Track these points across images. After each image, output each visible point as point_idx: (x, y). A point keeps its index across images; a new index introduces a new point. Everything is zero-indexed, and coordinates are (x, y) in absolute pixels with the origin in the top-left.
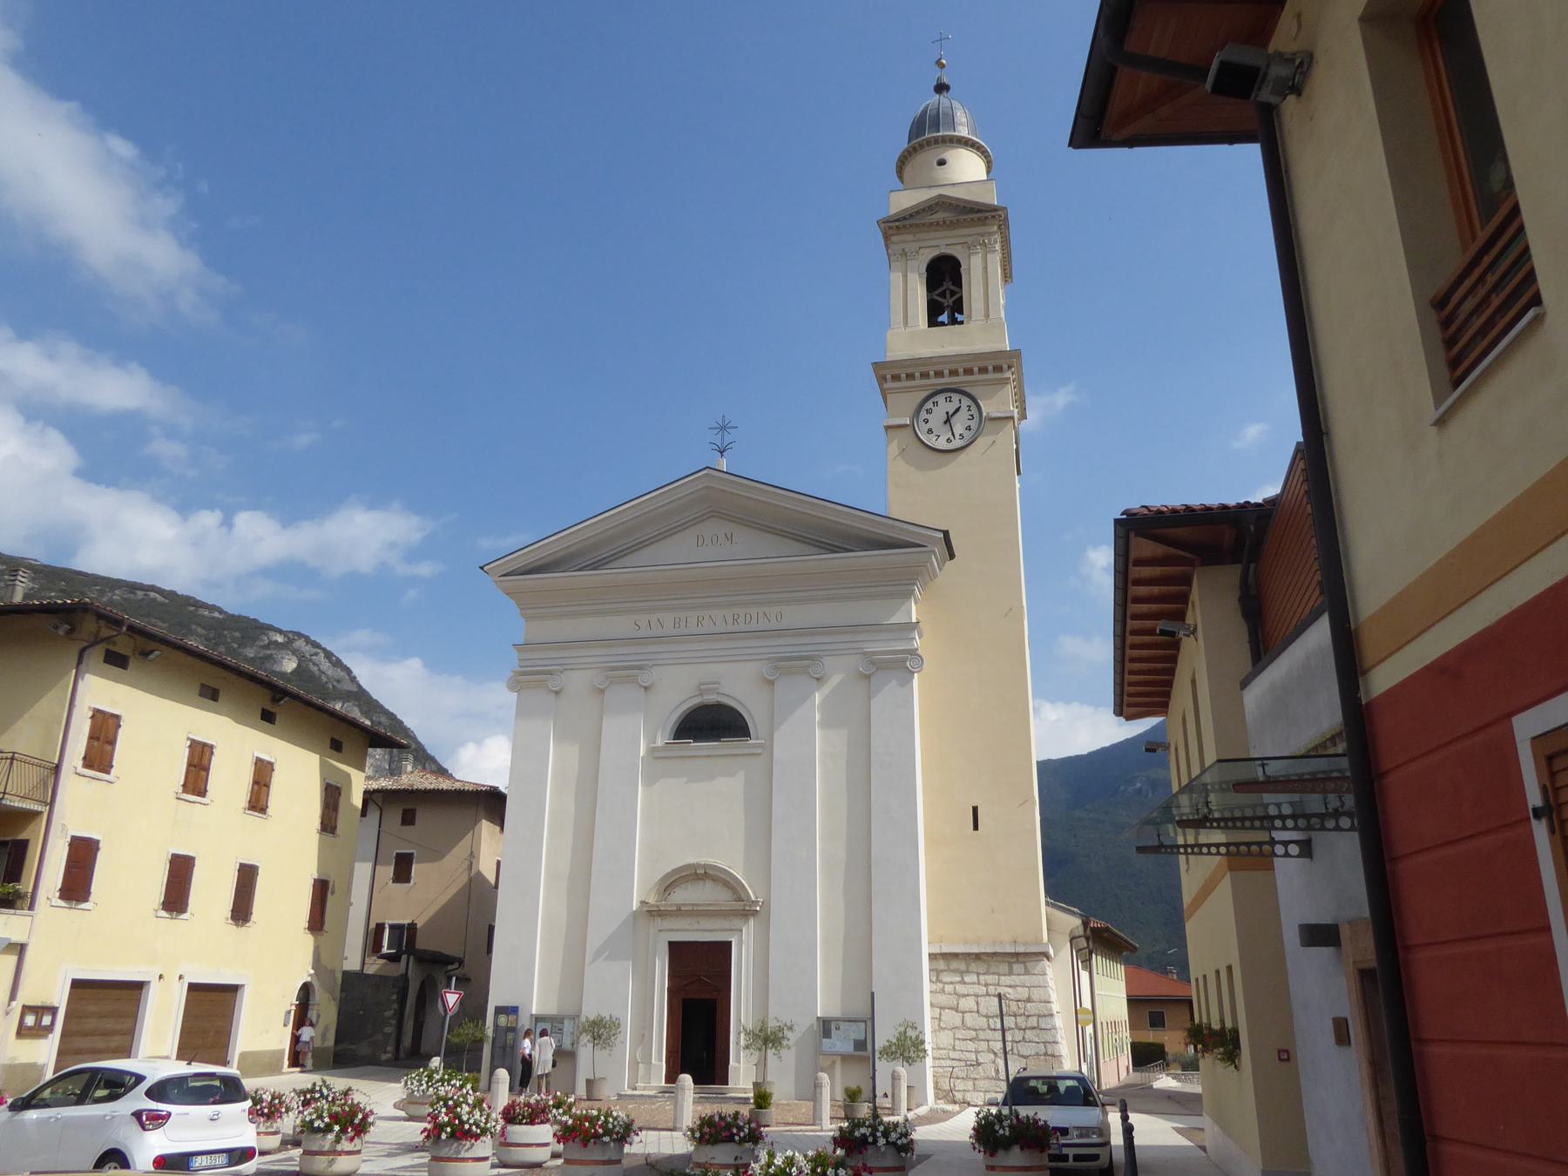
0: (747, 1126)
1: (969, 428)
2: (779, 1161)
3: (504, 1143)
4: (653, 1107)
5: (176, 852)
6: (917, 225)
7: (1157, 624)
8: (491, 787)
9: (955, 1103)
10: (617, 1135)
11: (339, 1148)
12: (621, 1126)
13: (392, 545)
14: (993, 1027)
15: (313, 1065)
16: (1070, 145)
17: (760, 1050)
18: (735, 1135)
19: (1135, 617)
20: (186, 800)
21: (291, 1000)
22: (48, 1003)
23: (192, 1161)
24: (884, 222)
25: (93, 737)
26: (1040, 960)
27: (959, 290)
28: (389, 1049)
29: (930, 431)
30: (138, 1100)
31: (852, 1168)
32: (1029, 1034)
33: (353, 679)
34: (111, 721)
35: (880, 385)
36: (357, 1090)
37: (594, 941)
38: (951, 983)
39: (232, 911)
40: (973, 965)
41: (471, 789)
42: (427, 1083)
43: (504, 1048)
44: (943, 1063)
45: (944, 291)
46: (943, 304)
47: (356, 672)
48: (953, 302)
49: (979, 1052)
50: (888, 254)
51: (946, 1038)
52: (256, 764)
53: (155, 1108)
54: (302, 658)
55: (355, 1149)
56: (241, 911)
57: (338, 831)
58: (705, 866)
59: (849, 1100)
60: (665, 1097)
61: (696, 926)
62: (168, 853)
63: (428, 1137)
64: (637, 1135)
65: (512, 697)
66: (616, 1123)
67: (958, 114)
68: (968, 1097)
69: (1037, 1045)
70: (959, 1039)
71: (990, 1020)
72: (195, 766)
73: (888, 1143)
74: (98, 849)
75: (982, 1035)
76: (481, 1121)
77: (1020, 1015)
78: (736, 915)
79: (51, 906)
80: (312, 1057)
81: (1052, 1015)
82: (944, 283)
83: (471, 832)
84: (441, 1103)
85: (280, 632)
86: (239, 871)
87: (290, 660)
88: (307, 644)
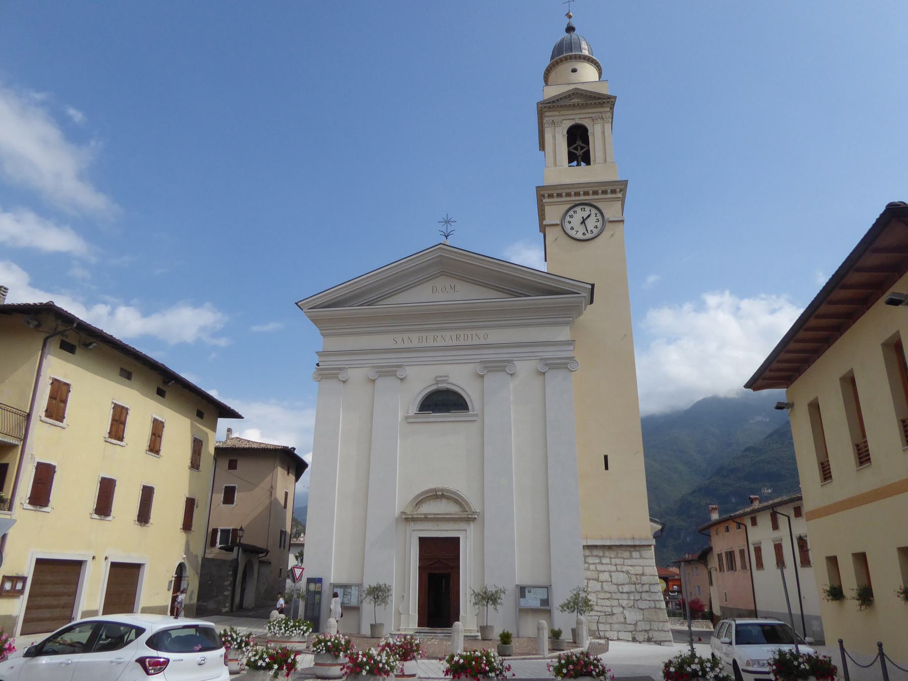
1: (596, 227)
5: (105, 477)
6: (561, 106)
8: (284, 447)
14: (621, 591)
18: (592, 670)
20: (111, 443)
21: (173, 574)
22: (20, 574)
24: (541, 104)
25: (52, 397)
28: (227, 605)
29: (572, 228)
30: (139, 649)
32: (645, 596)
34: (64, 387)
39: (138, 516)
40: (607, 552)
41: (272, 448)
42: (285, 628)
43: (314, 604)
48: (583, 153)
49: (613, 607)
52: (153, 422)
53: (156, 656)
56: (144, 516)
57: (201, 468)
58: (442, 490)
61: (436, 528)
62: (99, 477)
67: (583, 43)
68: (608, 635)
70: (600, 599)
72: (117, 421)
74: (55, 472)
75: (615, 596)
79: (23, 509)
83: (271, 474)
84: (323, 644)
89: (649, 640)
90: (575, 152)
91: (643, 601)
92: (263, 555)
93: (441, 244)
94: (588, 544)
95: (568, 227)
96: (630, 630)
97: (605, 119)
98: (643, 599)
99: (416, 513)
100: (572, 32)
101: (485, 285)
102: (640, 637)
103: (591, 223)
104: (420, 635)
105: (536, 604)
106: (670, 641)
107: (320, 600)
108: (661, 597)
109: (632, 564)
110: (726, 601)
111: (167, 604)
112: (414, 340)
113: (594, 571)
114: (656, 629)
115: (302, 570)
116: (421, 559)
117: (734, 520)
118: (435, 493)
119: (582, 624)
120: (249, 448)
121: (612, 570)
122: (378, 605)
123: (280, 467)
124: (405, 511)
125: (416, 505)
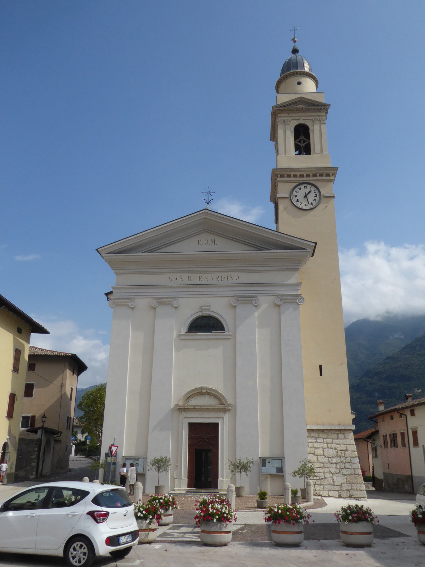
1: (315, 200)
6: (290, 110)
8: (72, 354)
14: (331, 462)
15: (7, 481)
24: (276, 107)
29: (298, 201)
32: (347, 465)
38: (312, 442)
40: (321, 434)
46: (300, 146)
48: (305, 145)
49: (325, 473)
53: (101, 510)
57: (20, 371)
58: (206, 389)
61: (201, 416)
68: (321, 493)
69: (351, 470)
71: (330, 459)
75: (326, 466)
77: (343, 457)
82: (301, 137)
83: (62, 374)
89: (350, 497)
91: (346, 469)
93: (205, 209)
95: (294, 200)
96: (337, 490)
97: (322, 121)
98: (346, 468)
99: (186, 405)
101: (228, 238)
102: (344, 494)
103: (311, 198)
104: (191, 494)
105: (274, 471)
106: (365, 497)
108: (358, 466)
109: (339, 443)
110: (389, 469)
113: (311, 447)
114: (355, 489)
115: (117, 447)
117: (398, 411)
118: (201, 391)
119: (311, 486)
121: (325, 447)
122: (160, 473)
123: (69, 369)
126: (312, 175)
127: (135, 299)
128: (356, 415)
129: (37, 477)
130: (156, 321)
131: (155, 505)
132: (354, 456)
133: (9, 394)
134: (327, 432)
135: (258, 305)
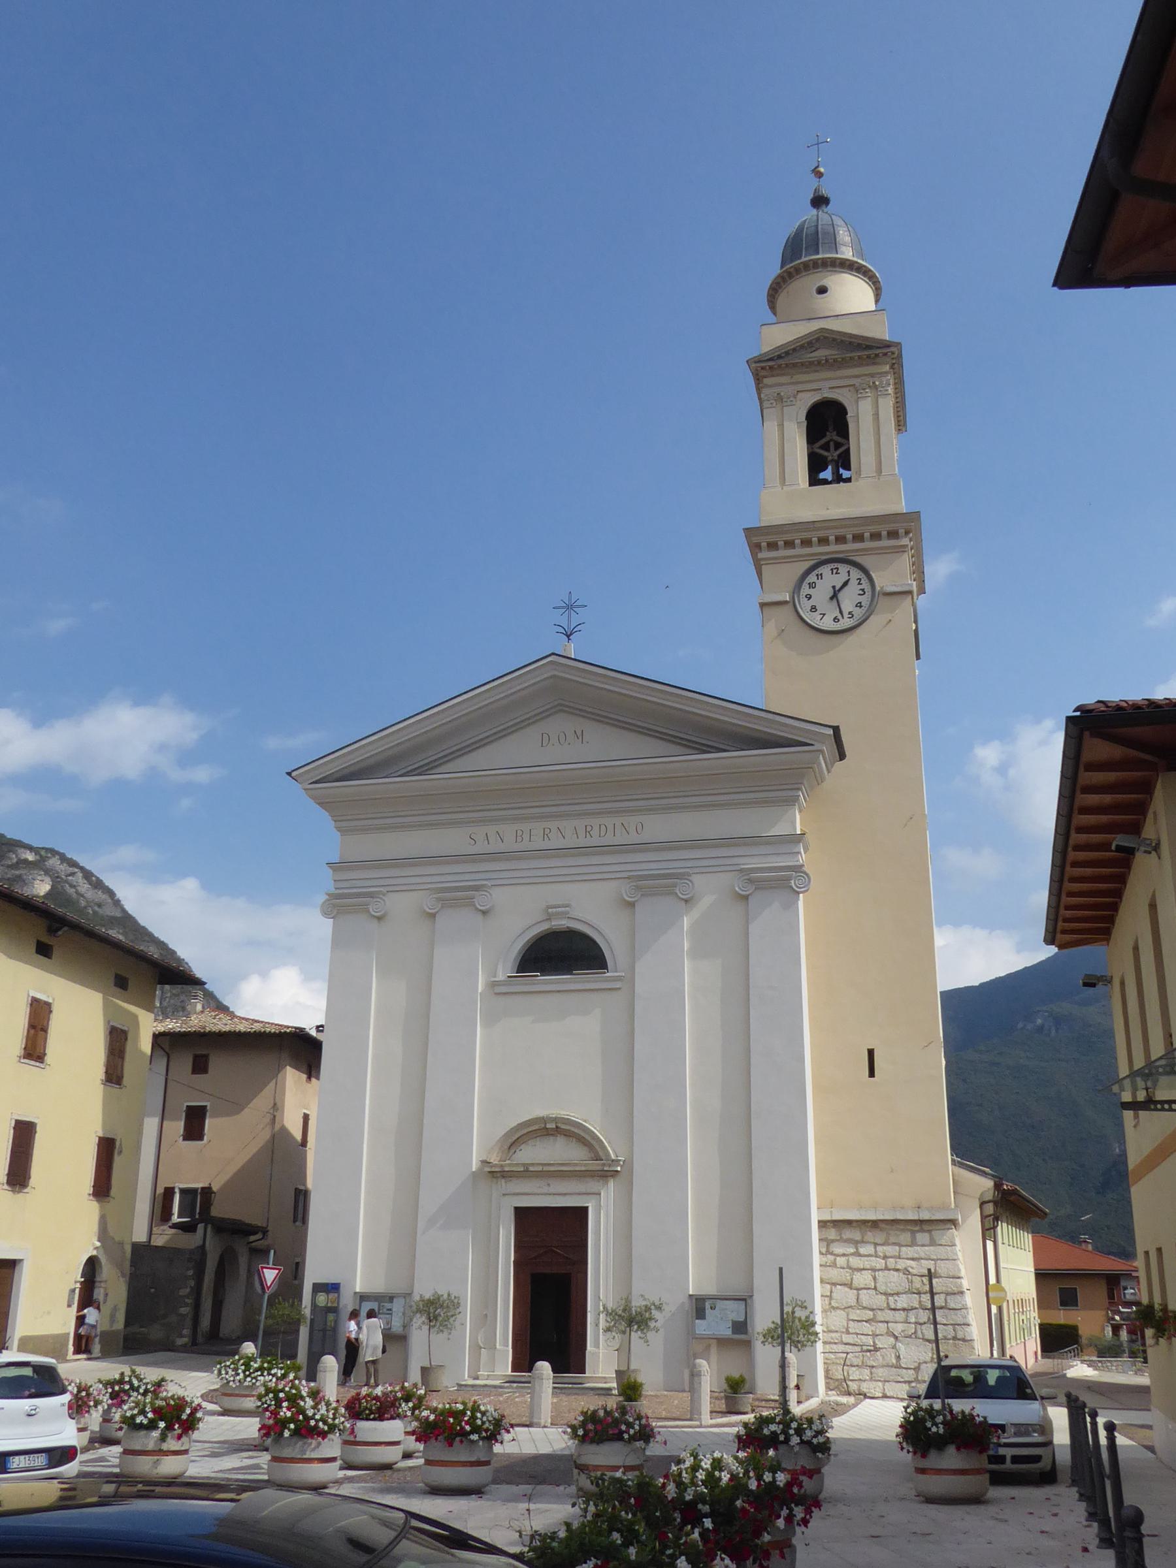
0: (637, 1422)
1: (859, 605)
2: (706, 1464)
3: (351, 1442)
4: (501, 1399)
6: (795, 365)
7: (1114, 839)
8: (296, 1028)
9: (849, 1394)
10: (486, 1433)
11: (165, 1447)
12: (490, 1422)
13: (162, 748)
14: (893, 1307)
15: (102, 1351)
16: (1054, 285)
17: (624, 1332)
19: (1080, 830)
21: (75, 1276)
23: (9, 1461)
24: (755, 362)
26: (949, 1229)
27: (846, 442)
29: (814, 609)
31: (789, 1471)
33: (117, 903)
35: (754, 556)
36: (172, 1381)
37: (429, 1204)
38: (844, 1255)
40: (869, 1233)
41: (273, 1031)
42: (244, 1372)
43: (324, 1330)
44: (835, 1348)
45: (828, 443)
46: (826, 458)
47: (120, 895)
49: (877, 1335)
50: (760, 399)
51: (838, 1319)
52: (31, 1005)
54: (56, 879)
55: (183, 1448)
57: (125, 1081)
58: (556, 1120)
59: (730, 1391)
60: (512, 1388)
61: (545, 1189)
63: (267, 1435)
64: (508, 1432)
65: (324, 927)
66: (485, 1419)
67: (841, 232)
68: (865, 1387)
70: (853, 1320)
71: (890, 1298)
73: (802, 1442)
75: (881, 1316)
76: (328, 1417)
78: (592, 1176)
80: (100, 1342)
81: (962, 1293)
82: (828, 433)
83: (274, 1081)
84: (271, 1395)
85: (30, 848)
86: (14, 1128)
87: (42, 881)
88: (62, 863)
90: (826, 454)
92: (259, 1236)
93: (553, 654)
94: (834, 1218)
96: (907, 1379)
99: (508, 1162)
100: (824, 206)
103: (848, 601)
105: (726, 1331)
107: (336, 1322)
109: (916, 1256)
111: (67, 1332)
112: (507, 836)
113: (844, 1268)
116: (519, 1247)
120: (230, 1031)
121: (878, 1267)
124: (488, 1160)
125: (509, 1148)
126: (851, 536)
127: (384, 895)
128: (997, 1180)
129: (194, 1343)
130: (435, 951)
131: (633, 1428)
132: (956, 1292)
133: (97, 1138)
134: (887, 1227)
135: (691, 898)
